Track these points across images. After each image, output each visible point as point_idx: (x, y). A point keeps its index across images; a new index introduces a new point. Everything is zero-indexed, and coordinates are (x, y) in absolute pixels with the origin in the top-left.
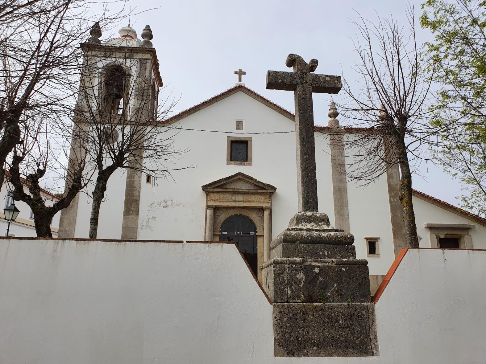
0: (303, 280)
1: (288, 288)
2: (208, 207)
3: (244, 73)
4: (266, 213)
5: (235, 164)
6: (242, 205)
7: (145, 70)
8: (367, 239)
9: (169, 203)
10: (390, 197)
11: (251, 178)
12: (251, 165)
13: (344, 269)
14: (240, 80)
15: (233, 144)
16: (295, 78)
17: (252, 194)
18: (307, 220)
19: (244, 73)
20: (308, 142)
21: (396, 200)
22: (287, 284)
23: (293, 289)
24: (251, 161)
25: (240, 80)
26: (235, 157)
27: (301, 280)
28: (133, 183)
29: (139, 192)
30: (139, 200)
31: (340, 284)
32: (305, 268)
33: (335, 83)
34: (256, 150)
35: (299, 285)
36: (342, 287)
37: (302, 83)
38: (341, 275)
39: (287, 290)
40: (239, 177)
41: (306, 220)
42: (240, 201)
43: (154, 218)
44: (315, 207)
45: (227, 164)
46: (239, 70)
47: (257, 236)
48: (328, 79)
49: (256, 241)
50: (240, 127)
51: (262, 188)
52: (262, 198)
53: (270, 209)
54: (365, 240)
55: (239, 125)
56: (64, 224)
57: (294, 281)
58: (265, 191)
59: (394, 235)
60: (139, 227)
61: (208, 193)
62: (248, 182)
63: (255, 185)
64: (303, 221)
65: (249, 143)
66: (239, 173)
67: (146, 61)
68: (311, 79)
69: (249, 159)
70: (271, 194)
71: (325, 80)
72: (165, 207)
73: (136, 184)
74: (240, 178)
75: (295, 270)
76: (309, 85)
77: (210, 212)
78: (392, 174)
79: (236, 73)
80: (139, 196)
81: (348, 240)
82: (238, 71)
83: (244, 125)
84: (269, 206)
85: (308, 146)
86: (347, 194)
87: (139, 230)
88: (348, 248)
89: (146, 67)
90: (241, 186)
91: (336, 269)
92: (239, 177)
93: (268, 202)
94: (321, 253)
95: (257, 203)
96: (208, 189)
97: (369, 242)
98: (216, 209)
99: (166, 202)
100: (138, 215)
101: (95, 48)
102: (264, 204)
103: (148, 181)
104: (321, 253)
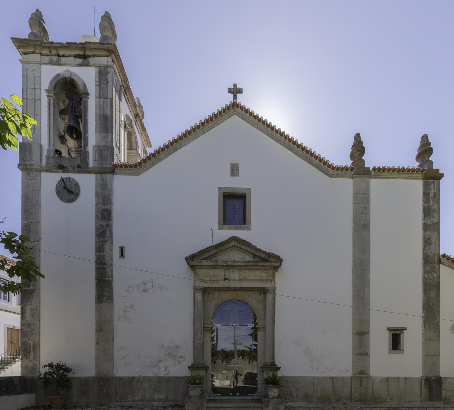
2: (196, 289)
4: (269, 296)
6: (237, 285)
7: (107, 86)
8: (389, 329)
9: (149, 285)
10: (424, 272)
12: (249, 229)
14: (235, 98)
15: (227, 201)
21: (431, 277)
25: (235, 98)
26: (230, 220)
28: (104, 258)
29: (112, 271)
30: (113, 282)
34: (256, 209)
40: (234, 243)
42: (235, 279)
43: (132, 306)
49: (122, 379)
51: (263, 259)
52: (264, 275)
54: (388, 332)
55: (234, 170)
56: (28, 315)
58: (268, 264)
59: (425, 324)
60: (115, 318)
61: (193, 267)
63: (254, 256)
66: (233, 237)
69: (247, 222)
70: (276, 268)
72: (144, 291)
73: (107, 260)
77: (199, 296)
78: (429, 239)
80: (112, 276)
82: (232, 87)
86: (370, 270)
87: (116, 322)
89: (107, 80)
92: (234, 243)
93: (271, 281)
96: (194, 261)
97: (393, 335)
98: (205, 291)
99: (145, 284)
100: (113, 302)
103: (122, 255)
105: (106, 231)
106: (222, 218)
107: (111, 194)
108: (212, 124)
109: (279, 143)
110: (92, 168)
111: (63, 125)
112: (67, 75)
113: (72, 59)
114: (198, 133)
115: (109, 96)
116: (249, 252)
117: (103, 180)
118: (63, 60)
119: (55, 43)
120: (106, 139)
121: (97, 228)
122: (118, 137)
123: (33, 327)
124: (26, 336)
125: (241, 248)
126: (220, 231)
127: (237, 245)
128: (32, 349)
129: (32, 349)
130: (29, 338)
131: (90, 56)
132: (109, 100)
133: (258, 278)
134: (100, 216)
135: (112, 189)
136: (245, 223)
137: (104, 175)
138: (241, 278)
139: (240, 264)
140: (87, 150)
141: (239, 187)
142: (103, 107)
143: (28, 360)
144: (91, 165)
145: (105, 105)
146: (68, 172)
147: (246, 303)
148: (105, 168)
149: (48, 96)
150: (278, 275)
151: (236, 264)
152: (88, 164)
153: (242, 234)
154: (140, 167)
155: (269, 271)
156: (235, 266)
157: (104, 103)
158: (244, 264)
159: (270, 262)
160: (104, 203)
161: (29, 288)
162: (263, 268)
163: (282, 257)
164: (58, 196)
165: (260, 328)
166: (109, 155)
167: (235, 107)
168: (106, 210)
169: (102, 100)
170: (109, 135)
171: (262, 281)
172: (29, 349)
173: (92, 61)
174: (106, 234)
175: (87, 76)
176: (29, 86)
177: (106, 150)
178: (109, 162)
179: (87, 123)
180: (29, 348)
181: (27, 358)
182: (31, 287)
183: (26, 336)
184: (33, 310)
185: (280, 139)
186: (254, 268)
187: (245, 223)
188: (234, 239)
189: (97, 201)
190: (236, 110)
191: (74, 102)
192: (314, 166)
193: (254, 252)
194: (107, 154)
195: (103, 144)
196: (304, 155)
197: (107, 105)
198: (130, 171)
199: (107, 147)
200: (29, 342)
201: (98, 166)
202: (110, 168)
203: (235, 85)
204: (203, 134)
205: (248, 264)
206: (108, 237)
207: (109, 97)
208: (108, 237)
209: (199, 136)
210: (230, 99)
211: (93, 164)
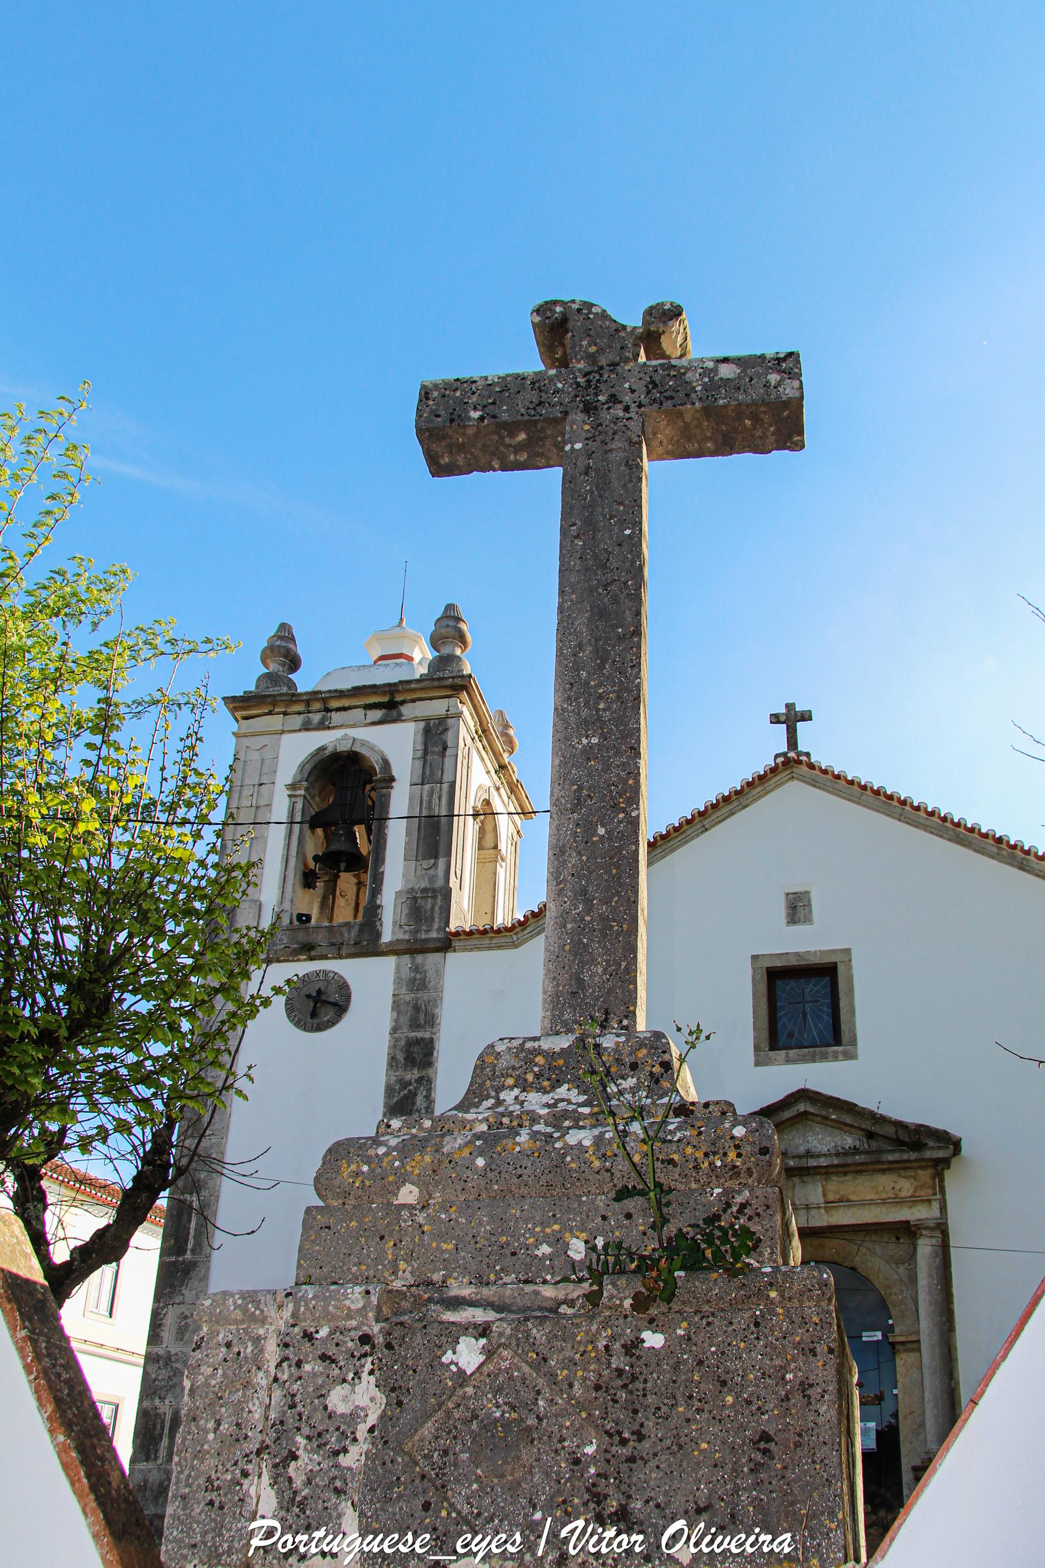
0: (372, 1419)
1: (266, 1479)
3: (806, 717)
4: (925, 1248)
5: (788, 1061)
11: (849, 1108)
12: (850, 1056)
13: (653, 1340)
16: (557, 391)
17: (859, 1170)
18: (538, 1076)
19: (806, 717)
20: (601, 667)
22: (258, 1453)
23: (299, 1482)
24: (853, 1042)
26: (791, 1035)
27: (354, 1416)
31: (624, 1442)
32: (389, 1346)
33: (767, 385)
35: (336, 1453)
36: (631, 1459)
37: (589, 409)
38: (634, 1378)
39: (253, 1491)
40: (802, 1107)
41: (530, 1077)
44: (618, 1005)
45: (757, 1064)
46: (787, 706)
47: (893, 1345)
48: (726, 371)
50: (801, 913)
52: (905, 1187)
53: (942, 1229)
55: (797, 908)
56: (167, 1335)
57: (306, 1431)
62: (840, 1125)
63: (870, 1135)
64: (510, 1081)
65: (841, 970)
66: (799, 1091)
67: (446, 724)
68: (640, 387)
69: (845, 1037)
70: (940, 1166)
71: (711, 380)
74: (806, 1113)
75: (324, 1357)
76: (627, 409)
79: (775, 719)
81: (732, 1155)
83: (813, 903)
84: (935, 1211)
85: (600, 685)
88: (728, 1205)
90: (821, 1141)
91: (601, 1344)
92: (802, 1107)
93: (929, 1201)
94: (545, 1249)
95: (884, 1209)
101: (274, 704)
102: (914, 1210)
104: (545, 1249)
105: (416, 1095)
106: (765, 1034)
107: (436, 1002)
108: (730, 807)
109: (926, 830)
110: (391, 943)
111: (315, 844)
112: (344, 747)
113: (361, 711)
114: (688, 833)
115: (447, 777)
116: (852, 1126)
117: (416, 969)
118: (336, 717)
119: (325, 692)
120: (432, 872)
121: (389, 1090)
122: (460, 856)
123: (179, 1365)
124: (155, 1393)
125: (827, 1118)
126: (758, 1068)
127: (812, 1111)
128: (166, 1431)
129: (166, 1431)
130: (162, 1399)
131: (403, 703)
132: (445, 786)
133: (884, 1196)
134: (401, 1057)
135: (439, 989)
136: (837, 1040)
137: (419, 958)
138: (831, 1197)
139: (823, 1162)
140: (378, 902)
141: (812, 949)
142: (430, 802)
143: (150, 1465)
144: (387, 935)
145: (435, 796)
146: (325, 957)
147: (853, 1269)
148: (427, 940)
149: (289, 796)
150: (950, 1179)
151: (812, 1162)
152: (379, 935)
153: (824, 1076)
154: (523, 930)
155: (921, 1172)
156: (808, 1168)
157: (431, 793)
158: (836, 1162)
159: (924, 1151)
160: (415, 1025)
161: (181, 1259)
162: (899, 1165)
163: (954, 1131)
164: (289, 1017)
165: (902, 1343)
166: (437, 909)
167: (792, 764)
168: (418, 1041)
169: (427, 787)
170: (442, 862)
171: (898, 1201)
172: (157, 1432)
173: (406, 710)
174: (414, 1103)
175: (395, 744)
176: (247, 782)
177: (429, 901)
178: (436, 926)
179: (385, 841)
180: (159, 1426)
181: (147, 1459)
182: (188, 1256)
183: (155, 1393)
184: (186, 1317)
185: (928, 823)
186: (870, 1167)
187: (837, 1040)
188: (803, 1095)
189: (396, 1021)
190: (794, 770)
191: (349, 793)
192: (1038, 876)
193: (867, 1125)
194: (433, 908)
195: (424, 884)
196: (1004, 853)
197: (440, 798)
198: (494, 941)
199: (434, 891)
200: (161, 1411)
201: (407, 937)
202: (438, 940)
203: (790, 707)
204: (702, 832)
205: (849, 1160)
206: (419, 1111)
207: (445, 779)
208: (419, 1111)
209: (692, 839)
210: (777, 740)
211: (393, 933)
